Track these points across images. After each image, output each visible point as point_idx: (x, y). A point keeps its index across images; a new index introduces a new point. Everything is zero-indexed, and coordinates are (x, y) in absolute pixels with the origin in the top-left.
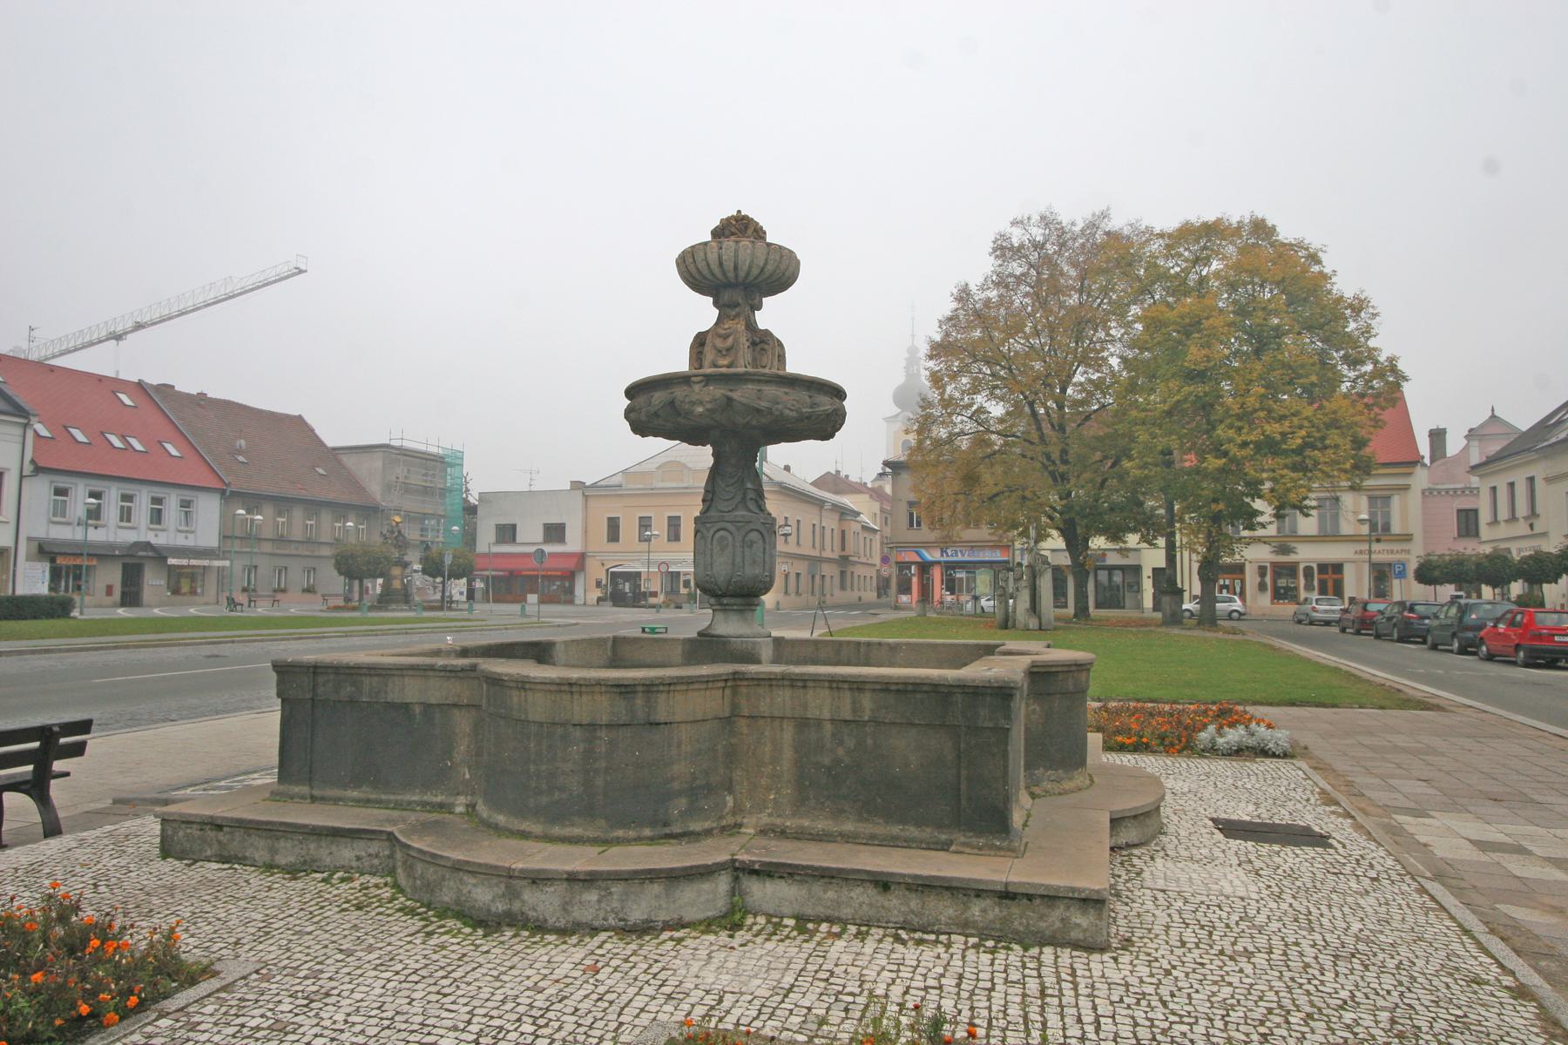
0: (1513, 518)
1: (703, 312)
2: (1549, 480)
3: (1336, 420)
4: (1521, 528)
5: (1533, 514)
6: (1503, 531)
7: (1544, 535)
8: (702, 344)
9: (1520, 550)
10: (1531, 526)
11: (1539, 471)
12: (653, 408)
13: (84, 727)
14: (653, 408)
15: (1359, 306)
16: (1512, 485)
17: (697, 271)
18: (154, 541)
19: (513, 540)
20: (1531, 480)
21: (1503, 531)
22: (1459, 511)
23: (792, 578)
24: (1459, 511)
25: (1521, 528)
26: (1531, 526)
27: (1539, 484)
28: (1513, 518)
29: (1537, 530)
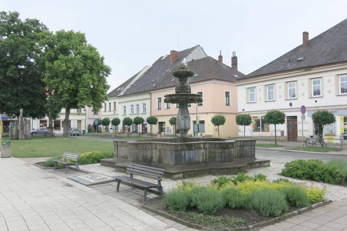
0: (110, 110)
2: (119, 103)
3: (333, 178)
4: (112, 113)
5: (115, 109)
6: (107, 113)
7: (118, 115)
8: (306, 34)
9: (112, 118)
10: (115, 113)
11: (117, 101)
12: (198, 99)
13: (269, 161)
14: (198, 99)
15: (3, 11)
16: (110, 103)
20: (115, 103)
21: (107, 113)
25: (112, 113)
26: (115, 113)
27: (117, 104)
28: (110, 110)
29: (116, 113)
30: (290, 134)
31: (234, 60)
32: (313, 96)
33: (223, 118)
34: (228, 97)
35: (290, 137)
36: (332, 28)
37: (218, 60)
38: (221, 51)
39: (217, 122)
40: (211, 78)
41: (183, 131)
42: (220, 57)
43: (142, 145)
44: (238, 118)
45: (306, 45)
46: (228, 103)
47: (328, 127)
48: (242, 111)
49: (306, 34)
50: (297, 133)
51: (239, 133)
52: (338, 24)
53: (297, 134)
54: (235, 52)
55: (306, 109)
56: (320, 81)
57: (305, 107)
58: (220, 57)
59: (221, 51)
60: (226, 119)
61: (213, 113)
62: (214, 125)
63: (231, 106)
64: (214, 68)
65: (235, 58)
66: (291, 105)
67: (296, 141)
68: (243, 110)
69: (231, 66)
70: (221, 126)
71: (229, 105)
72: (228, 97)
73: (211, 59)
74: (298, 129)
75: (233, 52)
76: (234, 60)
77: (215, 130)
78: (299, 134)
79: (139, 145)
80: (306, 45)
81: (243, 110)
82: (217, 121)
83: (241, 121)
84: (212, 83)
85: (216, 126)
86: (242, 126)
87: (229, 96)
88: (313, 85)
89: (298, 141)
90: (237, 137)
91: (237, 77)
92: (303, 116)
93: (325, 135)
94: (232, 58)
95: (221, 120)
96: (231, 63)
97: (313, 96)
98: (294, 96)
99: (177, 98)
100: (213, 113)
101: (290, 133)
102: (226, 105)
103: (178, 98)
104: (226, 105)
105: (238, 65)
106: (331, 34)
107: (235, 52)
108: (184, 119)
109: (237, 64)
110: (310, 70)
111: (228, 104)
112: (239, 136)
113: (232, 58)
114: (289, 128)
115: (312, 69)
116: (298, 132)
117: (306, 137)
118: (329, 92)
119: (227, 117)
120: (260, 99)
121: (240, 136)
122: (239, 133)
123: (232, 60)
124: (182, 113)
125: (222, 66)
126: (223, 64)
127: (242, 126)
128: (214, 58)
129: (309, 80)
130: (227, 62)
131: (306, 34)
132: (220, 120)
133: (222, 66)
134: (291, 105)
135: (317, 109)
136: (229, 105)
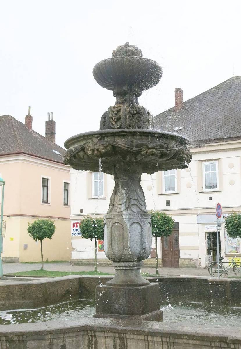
30: (166, 255)
31: (50, 125)
32: (205, 190)
33: (52, 225)
34: (45, 188)
35: (166, 259)
36: (212, 88)
37: (24, 123)
38: (30, 107)
39: (41, 234)
40: (18, 150)
41: (131, 264)
42: (29, 118)
43: (47, 342)
44: (87, 225)
45: (180, 109)
46: (45, 199)
47: (231, 242)
48: (79, 213)
49: (179, 92)
50: (179, 253)
51: (73, 253)
52: (221, 84)
53: (178, 254)
54: (52, 113)
55: (222, 209)
56: (216, 165)
57: (221, 206)
58: (29, 118)
59: (30, 107)
60: (56, 226)
61: (19, 217)
62: (34, 239)
63: (50, 205)
64: (19, 134)
65: (52, 123)
66: (168, 203)
67: (178, 266)
68: (82, 211)
69: (44, 135)
70: (46, 240)
71: (47, 202)
72: (45, 188)
73: (13, 120)
74: (180, 245)
75: (49, 113)
76: (50, 125)
77: (23, 248)
78: (183, 254)
79: (31, 344)
80: (180, 109)
81: (82, 211)
82: (41, 230)
83: (91, 231)
84: (20, 161)
85: (36, 241)
86: (92, 240)
87: (47, 187)
88: (204, 172)
89: (180, 266)
90: (59, 260)
91: (58, 154)
92: (219, 222)
93: (227, 255)
94: (46, 122)
95: (49, 229)
96: (45, 131)
97: (205, 190)
98: (173, 189)
99: (134, 144)
100: (21, 215)
101: (166, 252)
102: (43, 202)
103: (137, 146)
104: (43, 202)
105: (56, 135)
106: (216, 97)
107: (52, 113)
108: (139, 221)
109: (55, 134)
110: (201, 147)
111: (46, 201)
112: (72, 258)
113: (46, 122)
114: (165, 244)
115: (206, 145)
116: (180, 251)
117: (194, 259)
118: (189, 187)
119: (57, 224)
120: (189, 187)
121: (74, 258)
122: (73, 253)
123: (46, 124)
124: (129, 199)
125: (31, 134)
126: (33, 131)
127: (92, 240)
128: (18, 119)
129: (199, 161)
130: (39, 128)
131: (179, 92)
132: (46, 228)
133: (31, 134)
134: (168, 203)
135: (231, 210)
136: (47, 202)
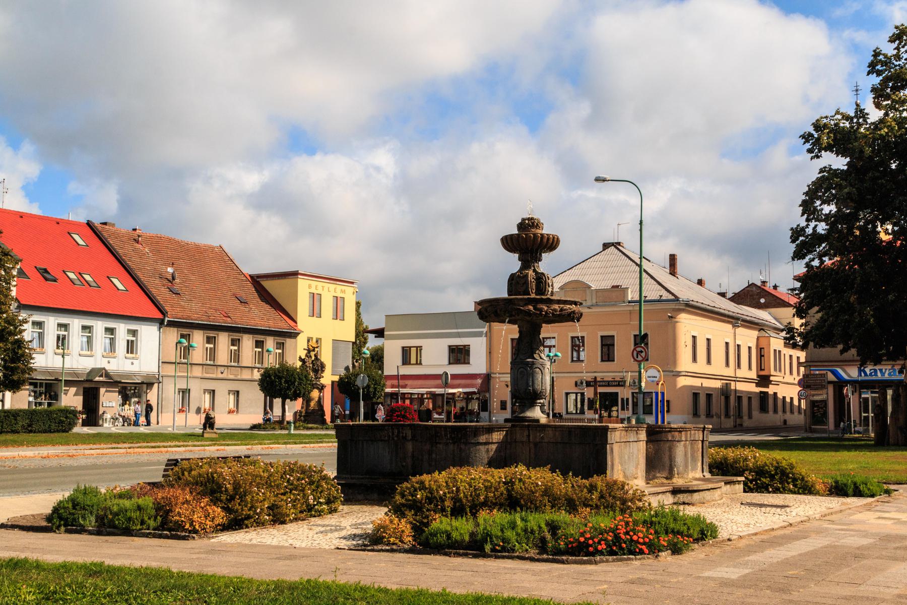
1: (512, 263)
17: (509, 243)
18: (109, 367)
19: (419, 363)
22: (450, 346)
23: (702, 400)
24: (450, 346)
